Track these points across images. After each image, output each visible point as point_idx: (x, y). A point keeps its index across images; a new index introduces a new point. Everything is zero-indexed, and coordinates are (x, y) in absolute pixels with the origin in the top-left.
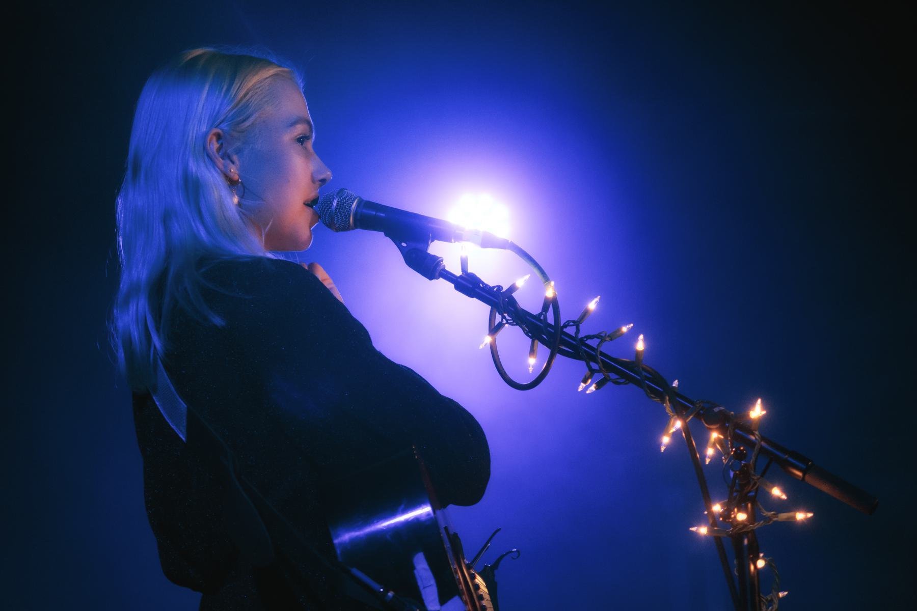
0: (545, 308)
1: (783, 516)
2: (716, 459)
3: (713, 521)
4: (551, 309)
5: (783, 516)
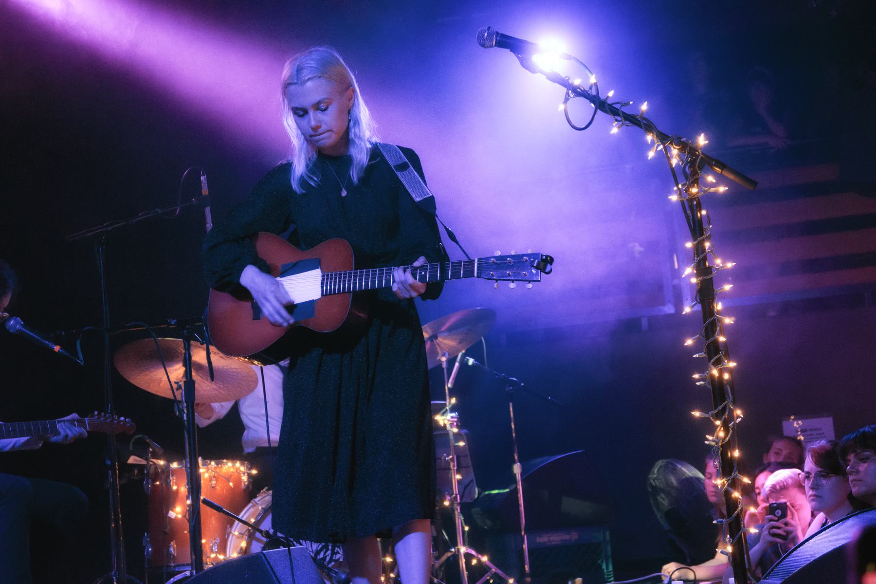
0: (591, 88)
1: (712, 190)
2: (677, 165)
3: (726, 312)
4: (594, 87)
5: (712, 190)
